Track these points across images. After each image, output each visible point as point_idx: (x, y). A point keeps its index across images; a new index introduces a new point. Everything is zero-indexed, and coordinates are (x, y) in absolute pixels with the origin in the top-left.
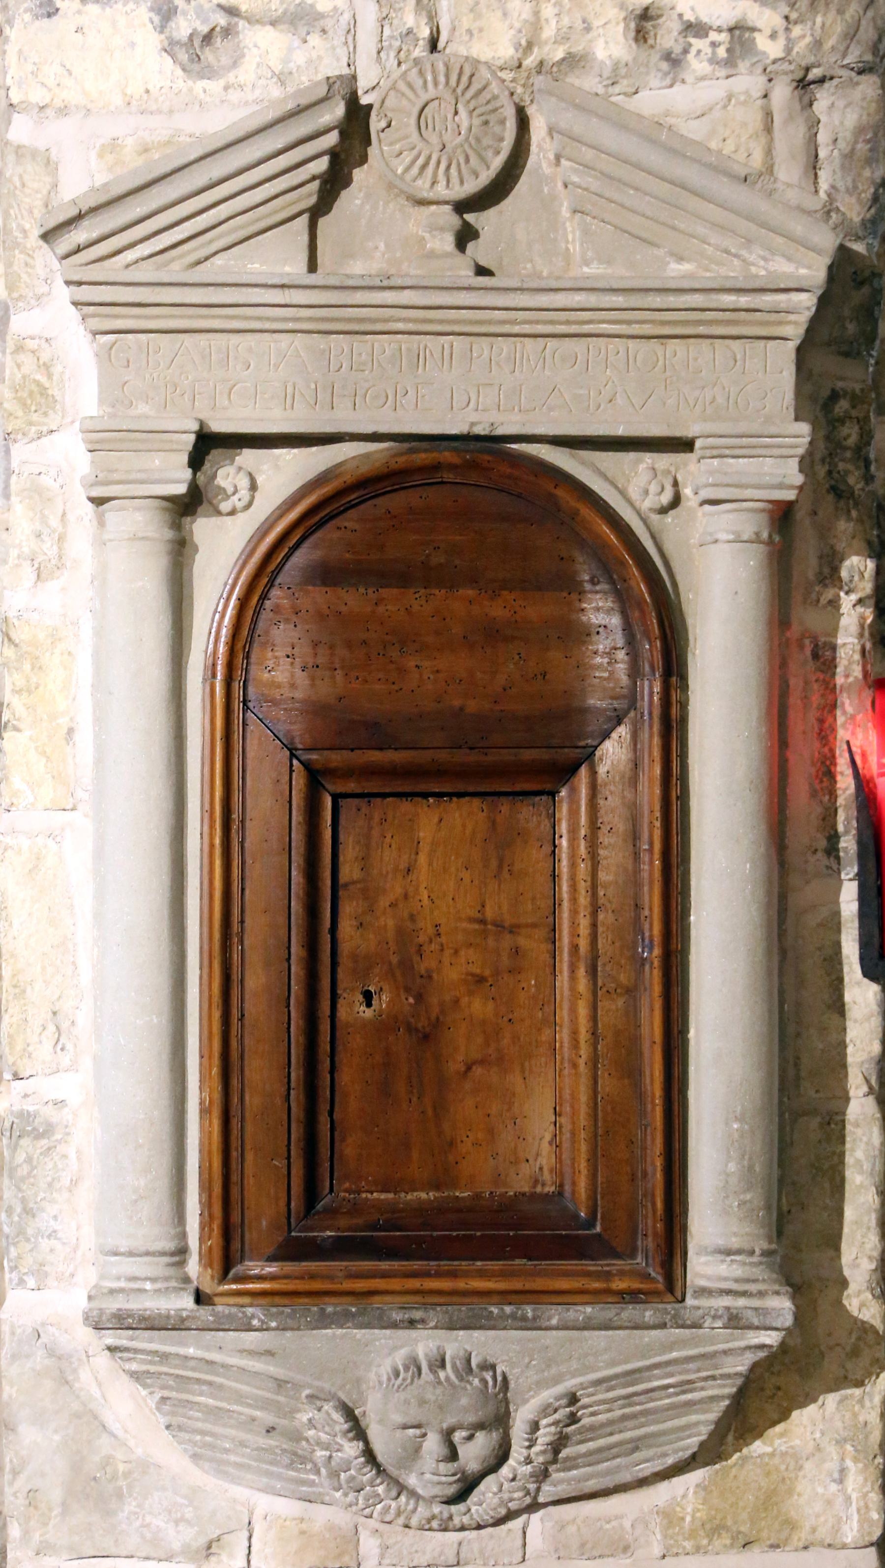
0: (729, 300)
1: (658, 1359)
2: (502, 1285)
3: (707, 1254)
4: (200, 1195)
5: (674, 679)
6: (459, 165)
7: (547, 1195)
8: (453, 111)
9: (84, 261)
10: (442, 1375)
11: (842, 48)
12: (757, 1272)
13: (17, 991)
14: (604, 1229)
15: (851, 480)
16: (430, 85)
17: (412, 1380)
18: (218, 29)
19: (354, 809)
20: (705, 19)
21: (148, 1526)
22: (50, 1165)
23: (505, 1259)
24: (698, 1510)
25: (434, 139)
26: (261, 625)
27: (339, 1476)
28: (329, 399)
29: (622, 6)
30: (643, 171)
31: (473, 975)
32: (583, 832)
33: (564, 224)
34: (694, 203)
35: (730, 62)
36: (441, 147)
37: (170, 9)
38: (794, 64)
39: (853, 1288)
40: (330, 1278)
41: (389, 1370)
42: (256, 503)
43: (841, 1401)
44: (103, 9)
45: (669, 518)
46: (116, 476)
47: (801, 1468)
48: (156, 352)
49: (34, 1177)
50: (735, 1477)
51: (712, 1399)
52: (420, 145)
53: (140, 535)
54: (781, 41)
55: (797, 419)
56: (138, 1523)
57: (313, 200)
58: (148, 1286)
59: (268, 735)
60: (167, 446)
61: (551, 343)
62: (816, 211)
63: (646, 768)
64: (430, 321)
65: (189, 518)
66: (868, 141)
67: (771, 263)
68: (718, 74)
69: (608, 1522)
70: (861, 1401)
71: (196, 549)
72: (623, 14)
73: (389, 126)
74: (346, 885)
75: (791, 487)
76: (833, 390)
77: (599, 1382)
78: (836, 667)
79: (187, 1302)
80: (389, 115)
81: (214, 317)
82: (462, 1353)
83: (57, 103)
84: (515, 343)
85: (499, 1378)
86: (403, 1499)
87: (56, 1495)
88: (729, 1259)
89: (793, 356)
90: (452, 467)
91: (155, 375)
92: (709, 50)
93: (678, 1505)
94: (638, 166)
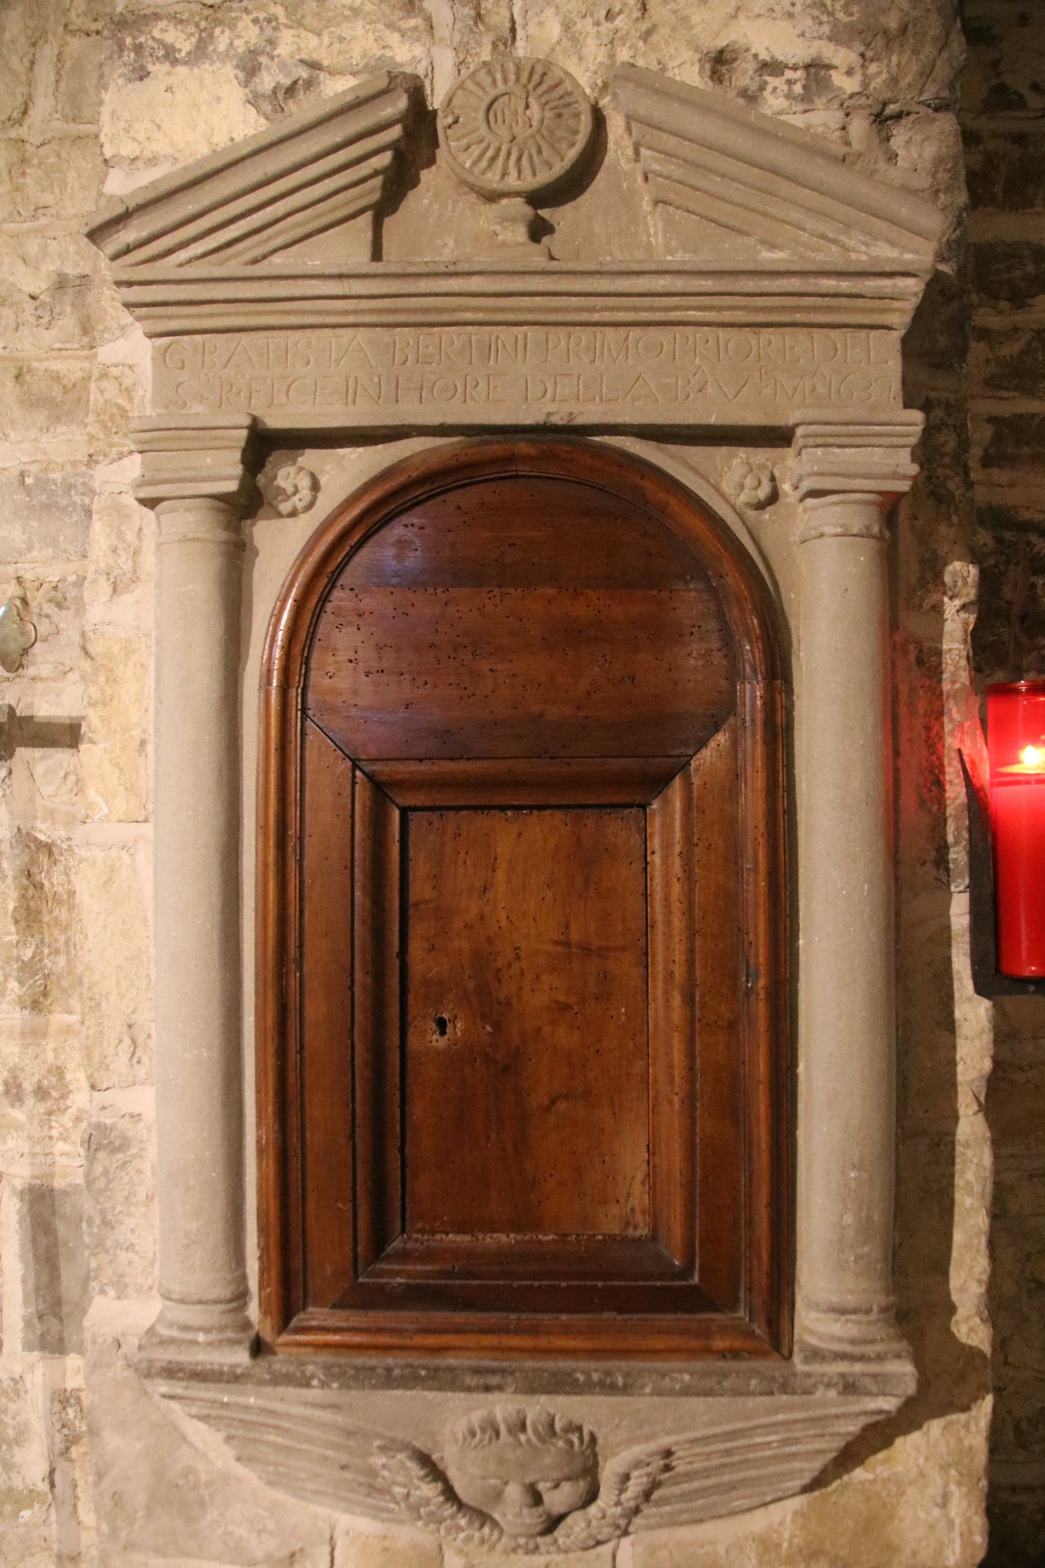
0: (828, 284)
1: (762, 1421)
2: (588, 1344)
3: (818, 1310)
4: (259, 1238)
5: (779, 682)
6: (531, 157)
7: (639, 1239)
8: (523, 104)
9: (133, 262)
10: (523, 1438)
11: (919, 86)
12: (877, 1331)
13: (92, 1004)
14: (701, 1280)
15: (951, 486)
16: (500, 83)
17: (490, 1442)
18: (301, 82)
19: (425, 823)
20: (781, 58)
21: (231, 1534)
22: (126, 1180)
23: (591, 1311)
24: (796, 1536)
25: (504, 132)
26: (322, 629)
27: (418, 1509)
28: (393, 393)
29: (697, 49)
30: (730, 156)
31: (556, 1002)
32: (678, 849)
33: (645, 217)
34: (786, 188)
35: (806, 97)
36: (510, 137)
37: (254, 66)
38: (871, 99)
39: (961, 1313)
40: (399, 1332)
41: (465, 1430)
42: (318, 503)
43: (945, 1427)
44: (192, 69)
45: (766, 515)
46: (165, 476)
47: (903, 1493)
48: (211, 353)
49: (111, 1190)
50: (835, 1503)
51: (819, 1452)
52: (489, 137)
53: (191, 536)
54: (858, 77)
55: (907, 405)
56: (221, 1531)
57: (376, 196)
58: (201, 1337)
59: (328, 746)
60: (217, 444)
61: (635, 333)
62: (923, 191)
63: (749, 780)
64: (501, 310)
65: (249, 522)
66: (948, 171)
67: (873, 248)
68: (794, 109)
69: (702, 1546)
70: (966, 1426)
71: (256, 552)
72: (698, 56)
73: (456, 122)
74: (417, 905)
75: (905, 477)
76: (927, 399)
77: (694, 1442)
78: (941, 673)
79: (241, 1357)
80: (456, 111)
81: (270, 313)
82: (544, 1417)
83: (147, 154)
84: (594, 333)
85: (586, 1438)
86: (486, 1530)
87: (141, 1499)
88: (843, 1318)
89: (899, 346)
90: (526, 459)
91: (210, 375)
92: (786, 88)
93: (776, 1532)
94: (724, 152)
